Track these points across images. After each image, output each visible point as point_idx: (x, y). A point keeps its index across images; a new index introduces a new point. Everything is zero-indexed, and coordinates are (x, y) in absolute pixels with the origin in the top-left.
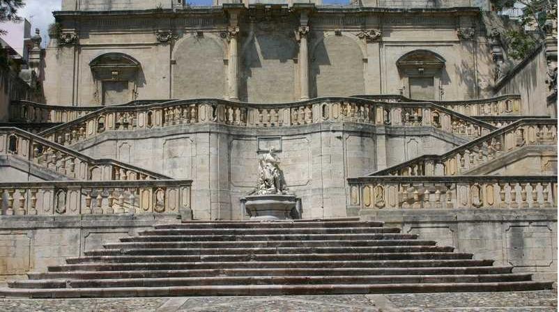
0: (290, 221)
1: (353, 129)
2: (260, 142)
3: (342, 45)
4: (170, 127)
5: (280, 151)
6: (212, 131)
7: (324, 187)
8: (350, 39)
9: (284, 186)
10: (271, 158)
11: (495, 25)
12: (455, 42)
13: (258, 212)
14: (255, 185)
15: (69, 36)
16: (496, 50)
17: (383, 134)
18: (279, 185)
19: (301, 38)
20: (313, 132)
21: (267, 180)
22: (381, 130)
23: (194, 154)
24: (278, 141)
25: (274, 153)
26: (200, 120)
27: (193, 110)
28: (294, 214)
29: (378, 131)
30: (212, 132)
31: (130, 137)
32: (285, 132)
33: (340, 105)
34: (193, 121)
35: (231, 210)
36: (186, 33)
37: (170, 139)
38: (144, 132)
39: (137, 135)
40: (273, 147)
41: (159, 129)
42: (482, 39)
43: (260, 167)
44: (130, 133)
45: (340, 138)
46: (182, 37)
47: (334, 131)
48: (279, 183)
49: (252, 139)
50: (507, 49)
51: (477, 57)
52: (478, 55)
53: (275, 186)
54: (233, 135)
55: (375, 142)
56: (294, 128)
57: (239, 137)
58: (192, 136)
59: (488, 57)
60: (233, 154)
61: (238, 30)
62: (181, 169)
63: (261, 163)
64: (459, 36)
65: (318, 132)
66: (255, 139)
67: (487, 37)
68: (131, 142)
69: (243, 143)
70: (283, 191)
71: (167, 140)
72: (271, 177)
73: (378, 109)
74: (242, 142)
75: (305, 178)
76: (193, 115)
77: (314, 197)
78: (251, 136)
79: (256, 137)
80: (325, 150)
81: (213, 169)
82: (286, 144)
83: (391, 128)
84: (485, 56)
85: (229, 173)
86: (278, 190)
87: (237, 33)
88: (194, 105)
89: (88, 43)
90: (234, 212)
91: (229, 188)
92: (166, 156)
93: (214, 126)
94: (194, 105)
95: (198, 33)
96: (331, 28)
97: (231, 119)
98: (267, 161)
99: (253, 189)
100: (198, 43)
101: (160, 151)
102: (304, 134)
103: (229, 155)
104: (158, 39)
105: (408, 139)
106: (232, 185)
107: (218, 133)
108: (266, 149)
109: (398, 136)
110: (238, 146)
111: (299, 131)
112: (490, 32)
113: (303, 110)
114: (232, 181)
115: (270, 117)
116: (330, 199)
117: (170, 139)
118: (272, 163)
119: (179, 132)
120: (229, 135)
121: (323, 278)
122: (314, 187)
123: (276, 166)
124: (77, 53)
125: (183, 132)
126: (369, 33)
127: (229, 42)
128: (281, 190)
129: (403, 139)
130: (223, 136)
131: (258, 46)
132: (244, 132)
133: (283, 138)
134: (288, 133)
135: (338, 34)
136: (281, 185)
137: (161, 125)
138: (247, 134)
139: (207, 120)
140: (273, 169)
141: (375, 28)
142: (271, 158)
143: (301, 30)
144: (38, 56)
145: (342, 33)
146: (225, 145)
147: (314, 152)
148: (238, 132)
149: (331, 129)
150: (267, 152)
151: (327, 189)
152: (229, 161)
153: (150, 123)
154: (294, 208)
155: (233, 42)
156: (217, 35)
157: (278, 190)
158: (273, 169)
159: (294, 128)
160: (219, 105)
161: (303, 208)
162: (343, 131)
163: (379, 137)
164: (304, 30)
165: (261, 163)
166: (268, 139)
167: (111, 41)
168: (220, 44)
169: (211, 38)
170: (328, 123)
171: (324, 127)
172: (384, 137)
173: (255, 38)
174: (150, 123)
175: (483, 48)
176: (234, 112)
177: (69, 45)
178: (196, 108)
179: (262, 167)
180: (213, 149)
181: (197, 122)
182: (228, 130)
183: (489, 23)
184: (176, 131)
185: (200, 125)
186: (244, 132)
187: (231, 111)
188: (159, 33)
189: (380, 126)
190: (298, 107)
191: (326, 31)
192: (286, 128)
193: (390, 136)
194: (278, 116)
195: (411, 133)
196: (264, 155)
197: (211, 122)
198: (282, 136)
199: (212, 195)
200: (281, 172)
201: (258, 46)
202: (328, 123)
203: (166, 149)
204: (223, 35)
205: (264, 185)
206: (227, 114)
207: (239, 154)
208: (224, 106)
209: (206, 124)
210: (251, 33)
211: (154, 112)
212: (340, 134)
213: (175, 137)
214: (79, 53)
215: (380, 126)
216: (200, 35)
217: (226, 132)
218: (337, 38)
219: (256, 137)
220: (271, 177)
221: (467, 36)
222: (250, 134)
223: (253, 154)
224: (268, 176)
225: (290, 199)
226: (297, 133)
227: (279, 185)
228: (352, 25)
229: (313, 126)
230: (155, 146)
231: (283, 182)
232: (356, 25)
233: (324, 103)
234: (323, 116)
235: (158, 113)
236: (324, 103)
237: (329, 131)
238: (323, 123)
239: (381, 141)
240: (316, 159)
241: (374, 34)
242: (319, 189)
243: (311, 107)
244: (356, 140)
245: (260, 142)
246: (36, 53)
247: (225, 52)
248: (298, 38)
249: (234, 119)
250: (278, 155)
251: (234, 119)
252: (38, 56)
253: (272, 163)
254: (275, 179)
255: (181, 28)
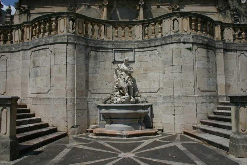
0: (142, 130)
1: (201, 42)
2: (116, 54)
3: (160, 12)
4: (36, 40)
5: (133, 62)
6: (70, 41)
7: (176, 95)
8: (165, 10)
9: (137, 93)
10: (125, 68)
11: (235, 5)
12: (216, 12)
13: (113, 120)
14: (111, 91)
15: (24, 8)
16: (236, 16)
17: (221, 48)
18: (132, 91)
19: (140, 8)
20: (163, 45)
21: (121, 88)
22: (220, 44)
23: (53, 63)
24: (131, 53)
25: (128, 63)
26: (59, 32)
27: (54, 23)
28: (147, 121)
29: (217, 45)
30: (70, 43)
31: (7, 50)
32: (138, 45)
33: (189, 19)
34: (52, 33)
35: (88, 116)
36: (82, 6)
37: (35, 51)
38: (18, 46)
39: (12, 49)
40: (126, 58)
41: (28, 43)
42: (229, 12)
43: (115, 76)
44: (7, 47)
45: (190, 49)
46: (80, 8)
47: (184, 43)
48: (132, 90)
49: (108, 51)
50: (240, 17)
51: (226, 20)
52: (227, 19)
53: (129, 94)
54: (91, 47)
55: (215, 53)
56: (145, 41)
57: (97, 49)
58: (51, 47)
59: (232, 20)
60: (91, 64)
61: (107, 3)
62: (42, 77)
63: (116, 72)
64: (217, 9)
65: (169, 44)
66: (111, 51)
67: (231, 11)
68: (7, 55)
69: (100, 55)
70: (136, 98)
71: (32, 52)
72: (125, 86)
73: (216, 27)
74: (100, 54)
75: (156, 86)
76: (53, 27)
77: (165, 105)
78: (107, 49)
79: (112, 49)
80: (175, 61)
81: (69, 78)
82: (139, 56)
83: (226, 44)
84: (230, 19)
85: (87, 81)
86: (132, 97)
87: (107, 5)
88: (54, 19)
89: (34, 12)
90: (90, 117)
91: (87, 95)
92: (32, 66)
93: (72, 38)
94: (54, 19)
95: (88, 6)
96: (155, 4)
97: (90, 33)
98: (122, 70)
99: (109, 95)
100: (88, 12)
101: (28, 61)
102: (155, 46)
103: (87, 65)
104: (68, 9)
105: (239, 53)
106: (89, 93)
107: (76, 44)
108: (120, 60)
109: (231, 51)
110: (96, 57)
111: (150, 43)
112: (232, 8)
113: (154, 25)
114: (89, 89)
115: (125, 32)
116: (180, 108)
117: (35, 51)
118: (126, 72)
119: (41, 43)
120: (87, 47)
121: (137, 110)
122: (165, 95)
123: (130, 75)
124: (28, 17)
125: (43, 43)
126: (174, 7)
127: (103, 10)
128: (134, 97)
129: (235, 53)
130: (81, 47)
131: (118, 13)
132: (101, 44)
133: (136, 50)
134: (141, 46)
135: (158, 7)
136: (134, 92)
137: (30, 39)
138: (104, 46)
139: (65, 33)
140: (127, 77)
141: (177, 4)
142: (125, 68)
143: (140, 3)
144: (9, 19)
145: (161, 7)
146: (82, 57)
147: (165, 63)
148: (97, 44)
149: (182, 40)
150: (122, 62)
151: (179, 97)
152: (87, 70)
153: (22, 38)
154: (147, 115)
155: (105, 9)
156: (97, 7)
157: (132, 97)
158: (127, 77)
159: (145, 41)
160: (78, 19)
161: (154, 113)
162: (193, 43)
163: (218, 51)
164: (142, 3)
165: (116, 72)
166: (122, 51)
167: (45, 11)
168: (98, 11)
169: (95, 9)
170: (178, 35)
171: (176, 39)
172: (222, 50)
173: (117, 9)
174: (22, 38)
175: (229, 15)
176: (93, 27)
177: (24, 13)
178: (56, 21)
179: (117, 76)
180: (70, 60)
181: (57, 34)
182: (87, 43)
183: (232, 4)
184: (39, 42)
185: (58, 36)
186: (101, 44)
187: (90, 26)
188: (68, 6)
189: (219, 41)
190: (149, 24)
191: (152, 6)
192: (138, 41)
193: (226, 50)
194: (131, 32)
195: (241, 49)
196: (119, 65)
197: (69, 34)
198: (135, 48)
199: (68, 103)
200: (134, 81)
201: (118, 13)
202: (178, 35)
203: (32, 60)
204: (101, 7)
205: (118, 93)
206: (86, 29)
207: (96, 64)
208: (83, 20)
209: (64, 35)
210: (115, 6)
211: (25, 28)
212: (190, 46)
213: (38, 48)
214: (30, 17)
215: (219, 41)
216: (89, 7)
217: (83, 43)
218: (158, 9)
219: (112, 49)
220: (125, 86)
221: (222, 9)
222: (106, 46)
223: (109, 64)
224: (123, 84)
225: (143, 108)
226: (148, 45)
227: (132, 91)
228: (165, 3)
229: (164, 38)
230: (24, 58)
231: (135, 89)
232: (167, 3)
233: (175, 17)
234: (173, 29)
235: (28, 28)
236: (175, 17)
237: (180, 42)
238: (174, 35)
239: (220, 54)
240: (167, 69)
241: (176, 7)
242: (170, 97)
243: (161, 23)
244: (202, 52)
245: (116, 54)
246: (8, 17)
247: (101, 15)
248: (138, 8)
249: (93, 34)
250: (132, 65)
251: (93, 34)
252: (9, 19)
253: (126, 72)
254: (129, 87)
255: (79, 4)
